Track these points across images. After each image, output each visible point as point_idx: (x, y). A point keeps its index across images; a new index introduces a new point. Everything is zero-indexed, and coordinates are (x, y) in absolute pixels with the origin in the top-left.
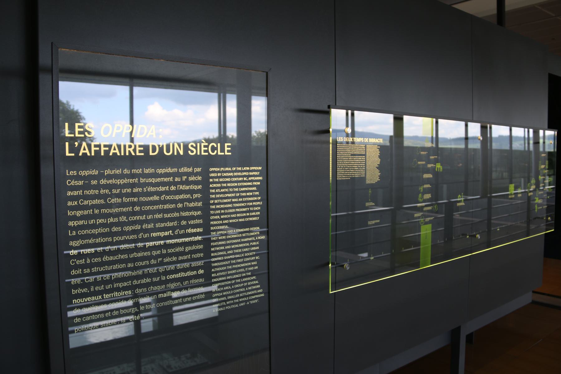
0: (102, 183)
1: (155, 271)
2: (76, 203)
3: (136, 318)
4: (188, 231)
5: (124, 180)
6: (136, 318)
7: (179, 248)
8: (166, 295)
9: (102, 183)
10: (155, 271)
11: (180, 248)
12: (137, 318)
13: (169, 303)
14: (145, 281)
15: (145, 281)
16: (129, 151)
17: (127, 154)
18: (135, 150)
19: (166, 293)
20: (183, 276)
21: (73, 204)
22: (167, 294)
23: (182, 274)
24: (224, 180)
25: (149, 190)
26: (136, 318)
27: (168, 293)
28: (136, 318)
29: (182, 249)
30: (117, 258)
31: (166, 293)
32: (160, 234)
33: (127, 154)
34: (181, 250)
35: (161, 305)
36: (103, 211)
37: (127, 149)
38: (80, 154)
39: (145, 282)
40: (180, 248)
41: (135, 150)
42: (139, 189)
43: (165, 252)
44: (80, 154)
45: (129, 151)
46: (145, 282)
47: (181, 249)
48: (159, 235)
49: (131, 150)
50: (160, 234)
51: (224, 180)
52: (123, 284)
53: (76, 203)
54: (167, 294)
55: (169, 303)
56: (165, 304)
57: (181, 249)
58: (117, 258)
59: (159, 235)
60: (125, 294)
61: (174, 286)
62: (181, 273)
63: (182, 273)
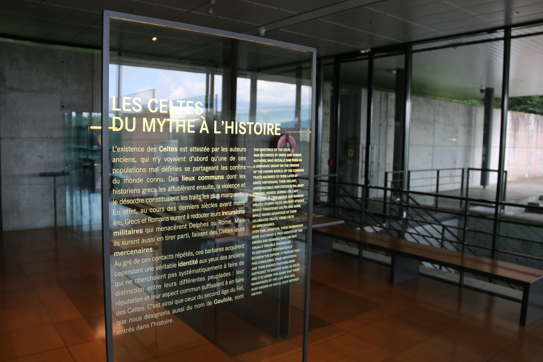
0: (164, 171)
1: (177, 190)
2: (217, 259)
3: (194, 263)
4: (117, 303)
5: (174, 226)
6: (194, 262)
7: (185, 253)
8: (130, 232)
9: (164, 171)
10: (177, 190)
11: (187, 253)
12: (195, 262)
13: (160, 200)
14: (171, 266)
15: (171, 266)
16: (270, 131)
17: (268, 134)
18: (274, 130)
19: (141, 249)
20: (194, 264)
21: (203, 262)
22: (120, 232)
23: (193, 262)
24: (265, 155)
25: (198, 189)
26: (194, 263)
27: (121, 231)
28: (194, 262)
29: (188, 254)
30: (121, 161)
31: (141, 249)
32: (208, 178)
33: (268, 134)
34: (187, 255)
35: (234, 168)
36: (150, 169)
37: (268, 129)
38: (201, 132)
39: (170, 267)
40: (187, 253)
41: (274, 130)
42: (170, 237)
43: (219, 187)
44: (201, 132)
45: (270, 131)
46: (170, 267)
47: (187, 254)
48: (207, 179)
49: (271, 130)
50: (208, 178)
51: (265, 155)
52: (181, 236)
53: (217, 259)
54: (120, 232)
55: (160, 200)
56: (167, 313)
57: (187, 254)
58: (121, 161)
59: (207, 179)
60: (146, 251)
61: (126, 264)
62: (191, 261)
63: (193, 261)
